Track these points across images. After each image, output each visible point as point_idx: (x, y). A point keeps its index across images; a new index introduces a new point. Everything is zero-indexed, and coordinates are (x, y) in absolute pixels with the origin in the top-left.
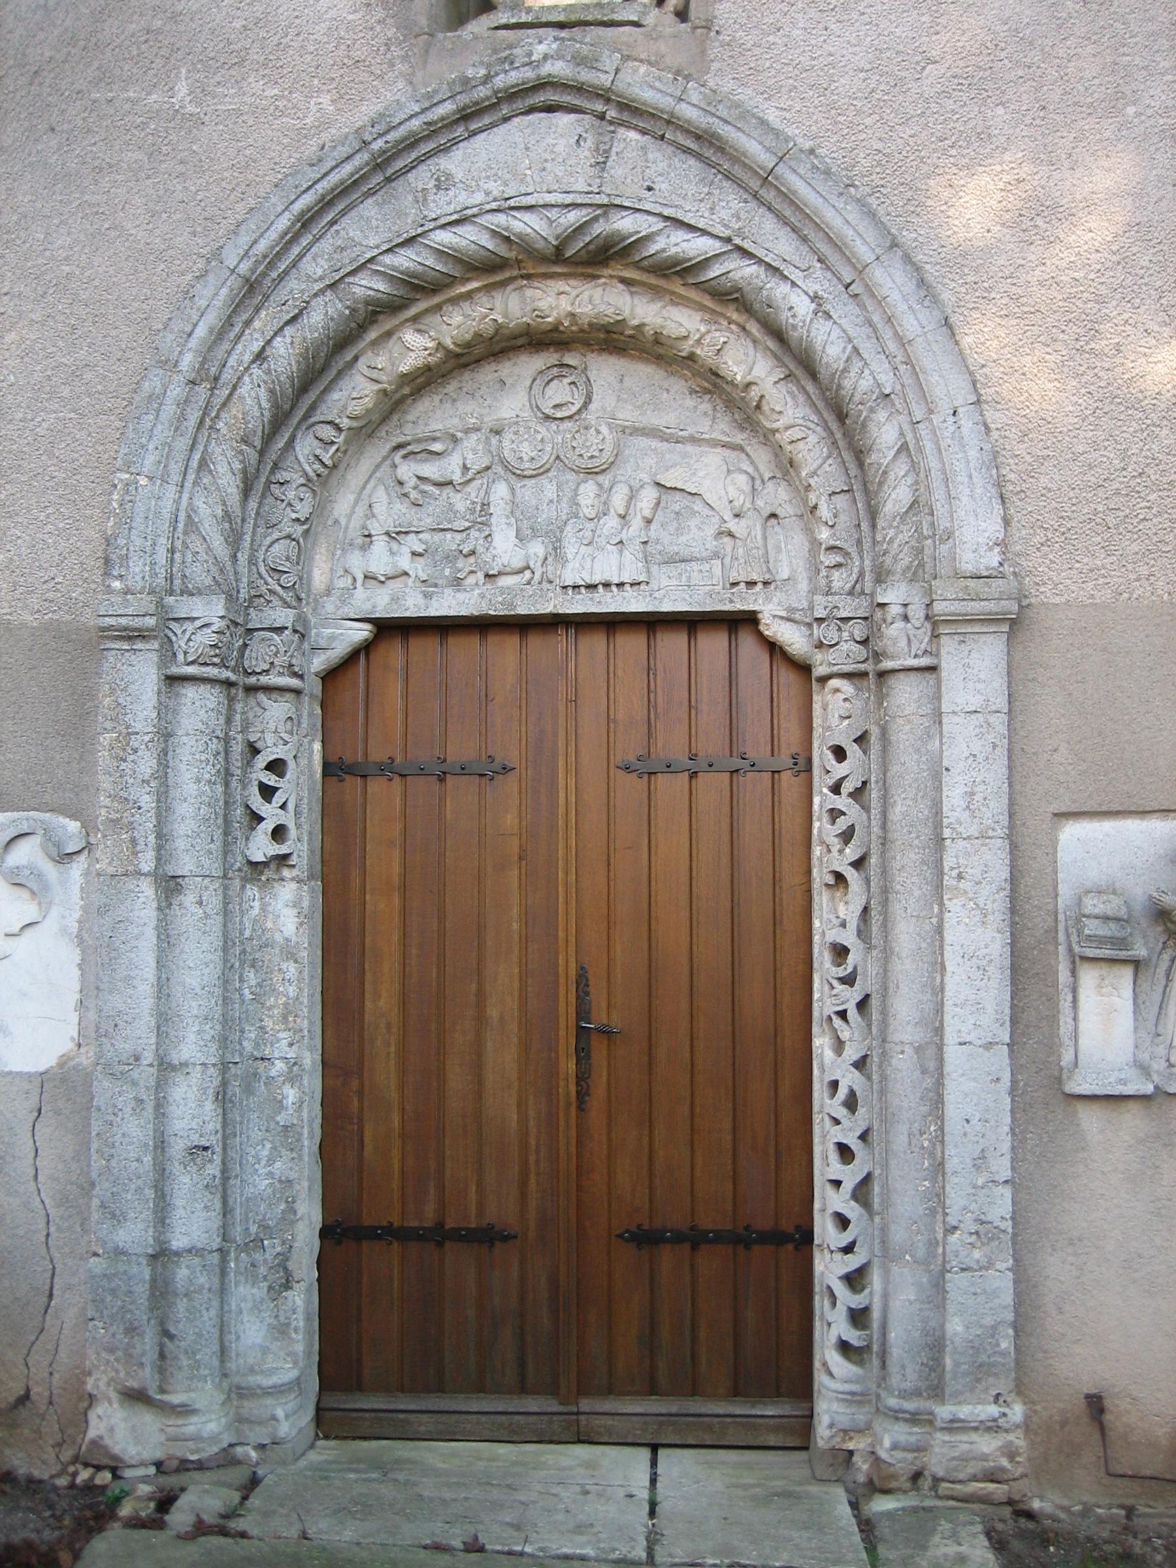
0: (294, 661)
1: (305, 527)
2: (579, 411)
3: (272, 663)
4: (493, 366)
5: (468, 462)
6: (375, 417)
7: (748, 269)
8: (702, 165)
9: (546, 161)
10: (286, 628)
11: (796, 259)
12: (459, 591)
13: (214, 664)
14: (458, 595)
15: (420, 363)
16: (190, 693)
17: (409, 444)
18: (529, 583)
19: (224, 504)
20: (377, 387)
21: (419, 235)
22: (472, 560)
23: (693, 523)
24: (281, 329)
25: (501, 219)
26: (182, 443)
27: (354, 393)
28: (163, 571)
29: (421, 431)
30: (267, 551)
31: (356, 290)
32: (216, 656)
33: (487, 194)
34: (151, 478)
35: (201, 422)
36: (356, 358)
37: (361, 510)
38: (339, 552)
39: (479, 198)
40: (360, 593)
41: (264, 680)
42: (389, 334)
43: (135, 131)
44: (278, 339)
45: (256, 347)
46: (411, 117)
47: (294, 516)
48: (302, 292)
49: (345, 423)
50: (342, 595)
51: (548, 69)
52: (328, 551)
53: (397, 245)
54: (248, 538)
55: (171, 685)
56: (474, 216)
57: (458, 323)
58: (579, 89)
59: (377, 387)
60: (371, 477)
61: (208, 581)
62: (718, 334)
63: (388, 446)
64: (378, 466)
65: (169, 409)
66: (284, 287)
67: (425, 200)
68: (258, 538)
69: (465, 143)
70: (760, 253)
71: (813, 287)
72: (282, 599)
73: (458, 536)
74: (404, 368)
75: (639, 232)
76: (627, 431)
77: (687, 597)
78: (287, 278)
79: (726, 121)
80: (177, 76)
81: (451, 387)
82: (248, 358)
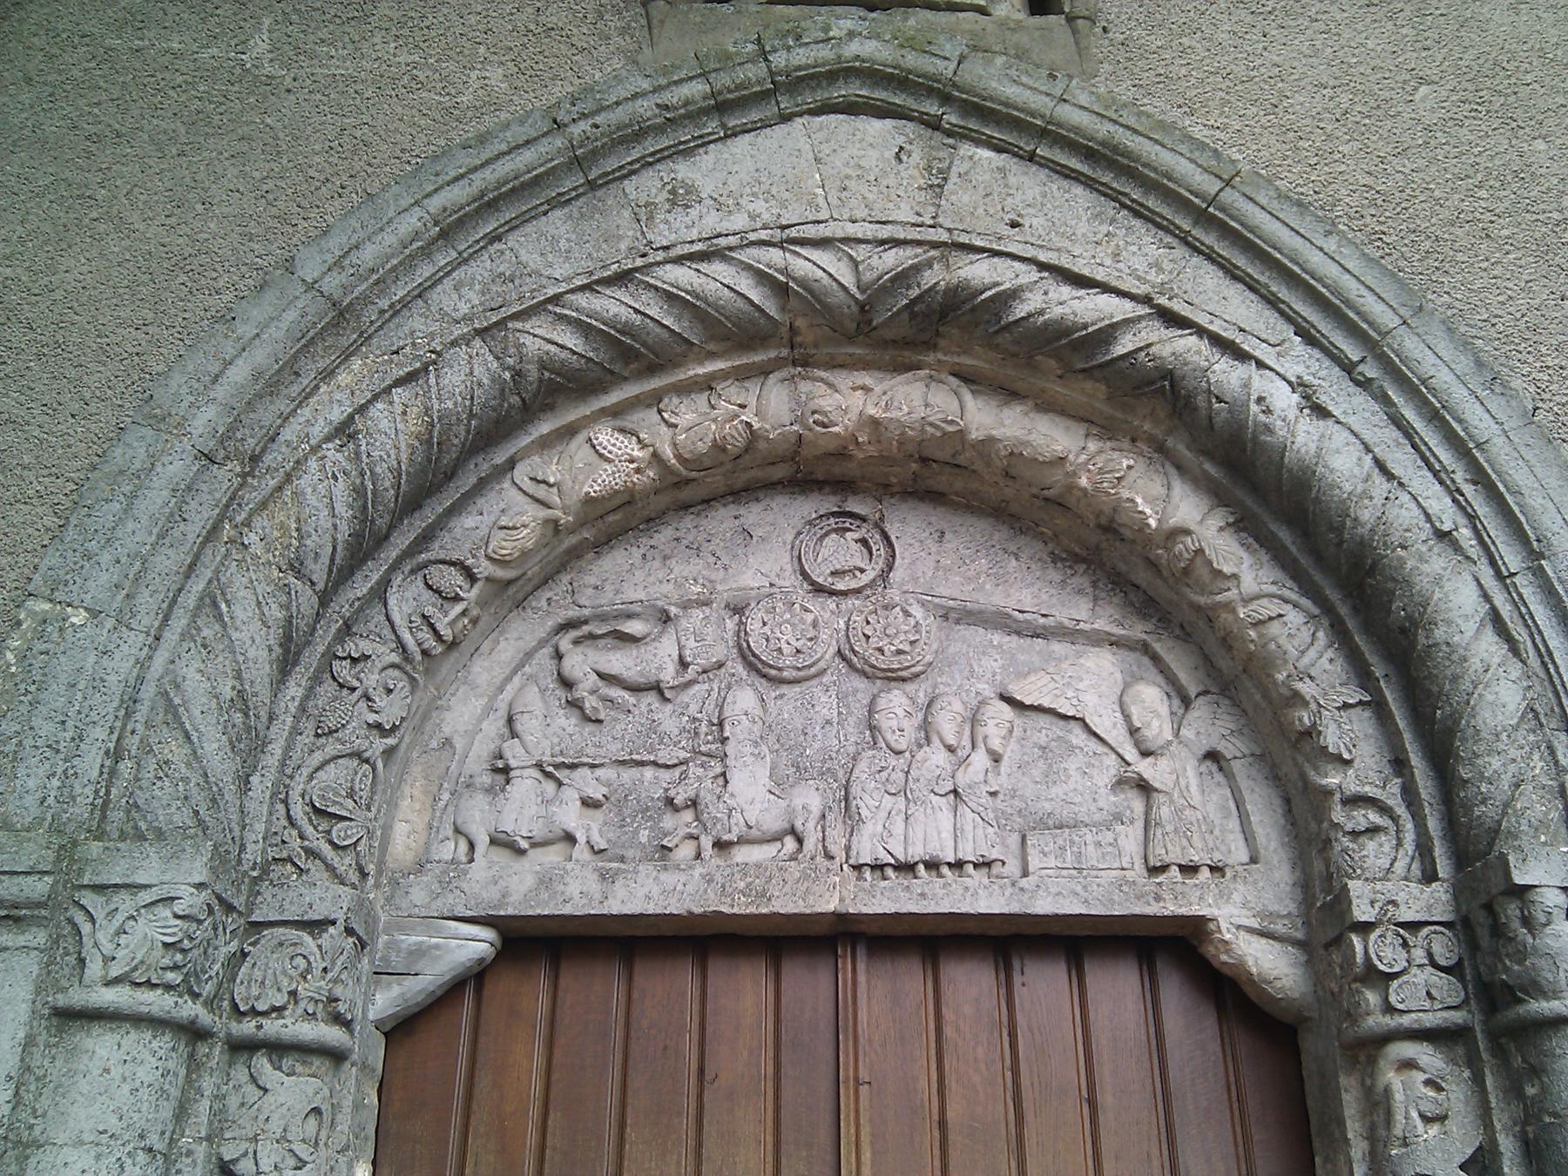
0: (338, 991)
1: (390, 741)
2: (872, 584)
3: (293, 994)
4: (732, 510)
5: (688, 652)
6: (533, 569)
7: (1182, 341)
8: (1095, 194)
9: (848, 177)
10: (333, 923)
11: (1259, 328)
12: (665, 868)
13: (168, 987)
14: (664, 876)
15: (618, 482)
16: (102, 1046)
17: (586, 622)
18: (793, 858)
19: (238, 676)
20: (544, 513)
21: (636, 270)
22: (688, 816)
23: (1073, 764)
24: (388, 390)
25: (775, 255)
26: (169, 561)
27: (504, 519)
28: (89, 791)
29: (607, 599)
30: (311, 778)
31: (527, 340)
32: (175, 967)
33: (753, 217)
34: (94, 613)
35: (215, 529)
36: (511, 464)
37: (494, 725)
38: (446, 796)
39: (739, 222)
40: (479, 870)
41: (272, 1028)
42: (570, 431)
43: (171, 93)
44: (380, 406)
45: (337, 415)
46: (635, 96)
47: (372, 717)
48: (432, 335)
49: (484, 568)
50: (445, 872)
51: (853, 48)
52: (426, 793)
53: (600, 282)
54: (277, 749)
55: (60, 1031)
56: (731, 249)
57: (693, 423)
58: (901, 81)
59: (544, 513)
60: (515, 672)
61: (183, 817)
62: (1116, 455)
63: (550, 624)
64: (529, 655)
65: (156, 498)
66: (399, 326)
67: (650, 218)
68: (296, 755)
69: (719, 145)
70: (1202, 319)
71: (1293, 370)
72: (330, 868)
73: (665, 775)
74: (593, 488)
75: (997, 284)
76: (953, 615)
77: (1079, 888)
78: (405, 312)
79: (1135, 131)
80: (258, 27)
81: (663, 537)
82: (319, 430)
